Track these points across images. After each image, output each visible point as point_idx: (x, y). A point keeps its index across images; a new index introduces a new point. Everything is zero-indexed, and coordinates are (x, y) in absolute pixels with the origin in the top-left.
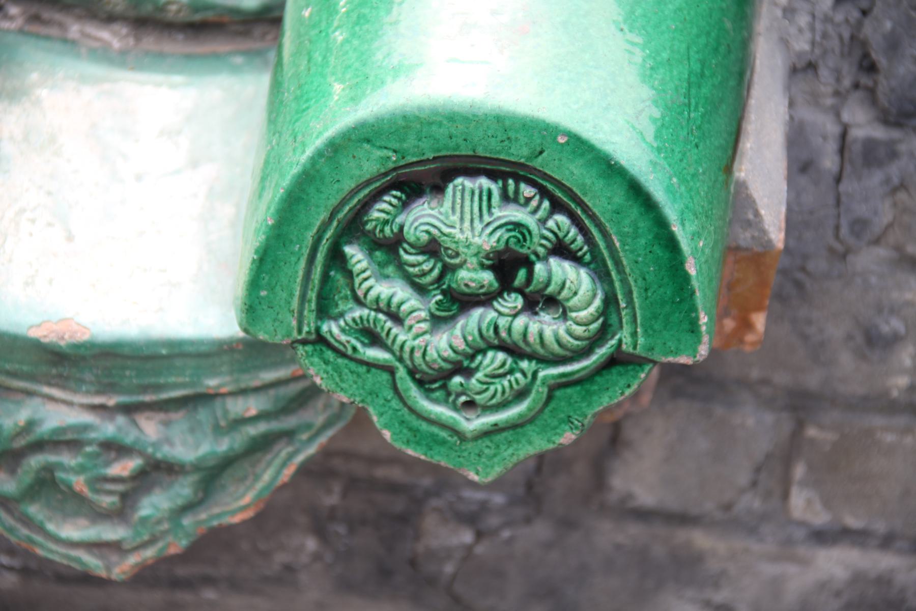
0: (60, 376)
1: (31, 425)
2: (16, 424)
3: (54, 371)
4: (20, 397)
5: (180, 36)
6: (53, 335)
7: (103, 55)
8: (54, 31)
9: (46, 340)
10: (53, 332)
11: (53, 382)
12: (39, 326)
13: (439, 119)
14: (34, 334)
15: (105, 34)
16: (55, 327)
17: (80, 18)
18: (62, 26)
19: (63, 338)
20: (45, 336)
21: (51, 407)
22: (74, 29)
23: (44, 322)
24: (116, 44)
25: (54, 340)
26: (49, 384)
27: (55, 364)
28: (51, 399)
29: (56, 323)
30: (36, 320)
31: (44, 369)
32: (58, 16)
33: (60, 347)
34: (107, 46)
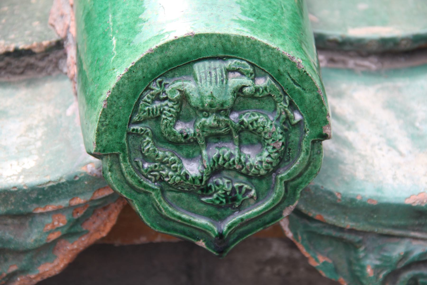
0: (420, 225)
1: (407, 254)
2: (399, 254)
3: (417, 222)
4: (396, 240)
5: (402, 59)
6: (417, 202)
7: (368, 73)
8: (340, 65)
9: (415, 205)
10: (418, 200)
11: (416, 228)
12: (409, 198)
13: (181, 210)
14: (408, 202)
15: (366, 63)
16: (417, 197)
17: (351, 57)
18: (344, 62)
19: (423, 203)
20: (414, 203)
21: (415, 243)
22: (351, 63)
23: (411, 196)
24: (374, 67)
25: (419, 204)
26: (414, 230)
27: (417, 218)
28: (416, 238)
29: (418, 195)
30: (407, 195)
31: (412, 221)
32: (341, 57)
33: (423, 207)
34: (369, 68)
